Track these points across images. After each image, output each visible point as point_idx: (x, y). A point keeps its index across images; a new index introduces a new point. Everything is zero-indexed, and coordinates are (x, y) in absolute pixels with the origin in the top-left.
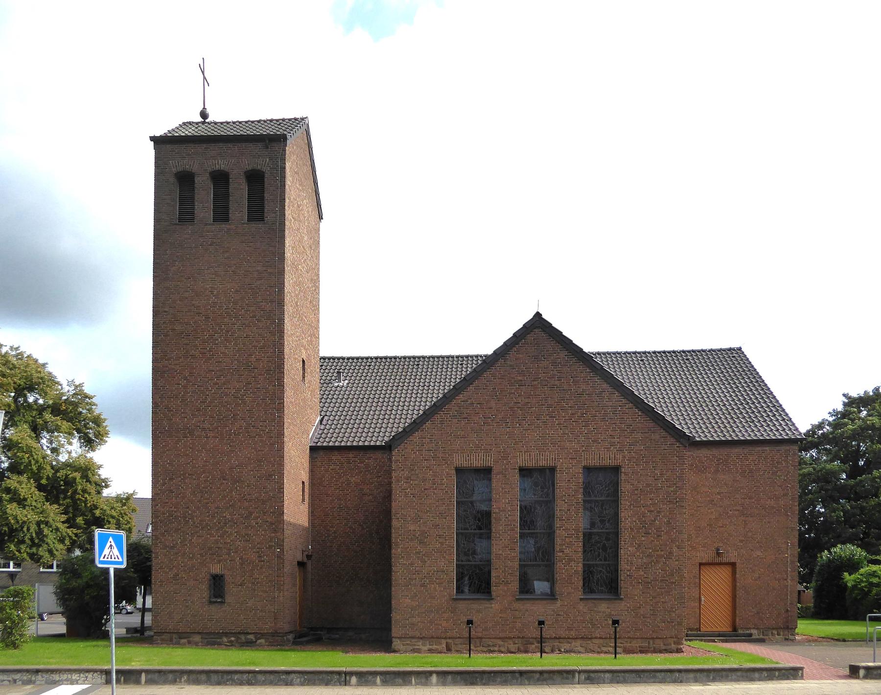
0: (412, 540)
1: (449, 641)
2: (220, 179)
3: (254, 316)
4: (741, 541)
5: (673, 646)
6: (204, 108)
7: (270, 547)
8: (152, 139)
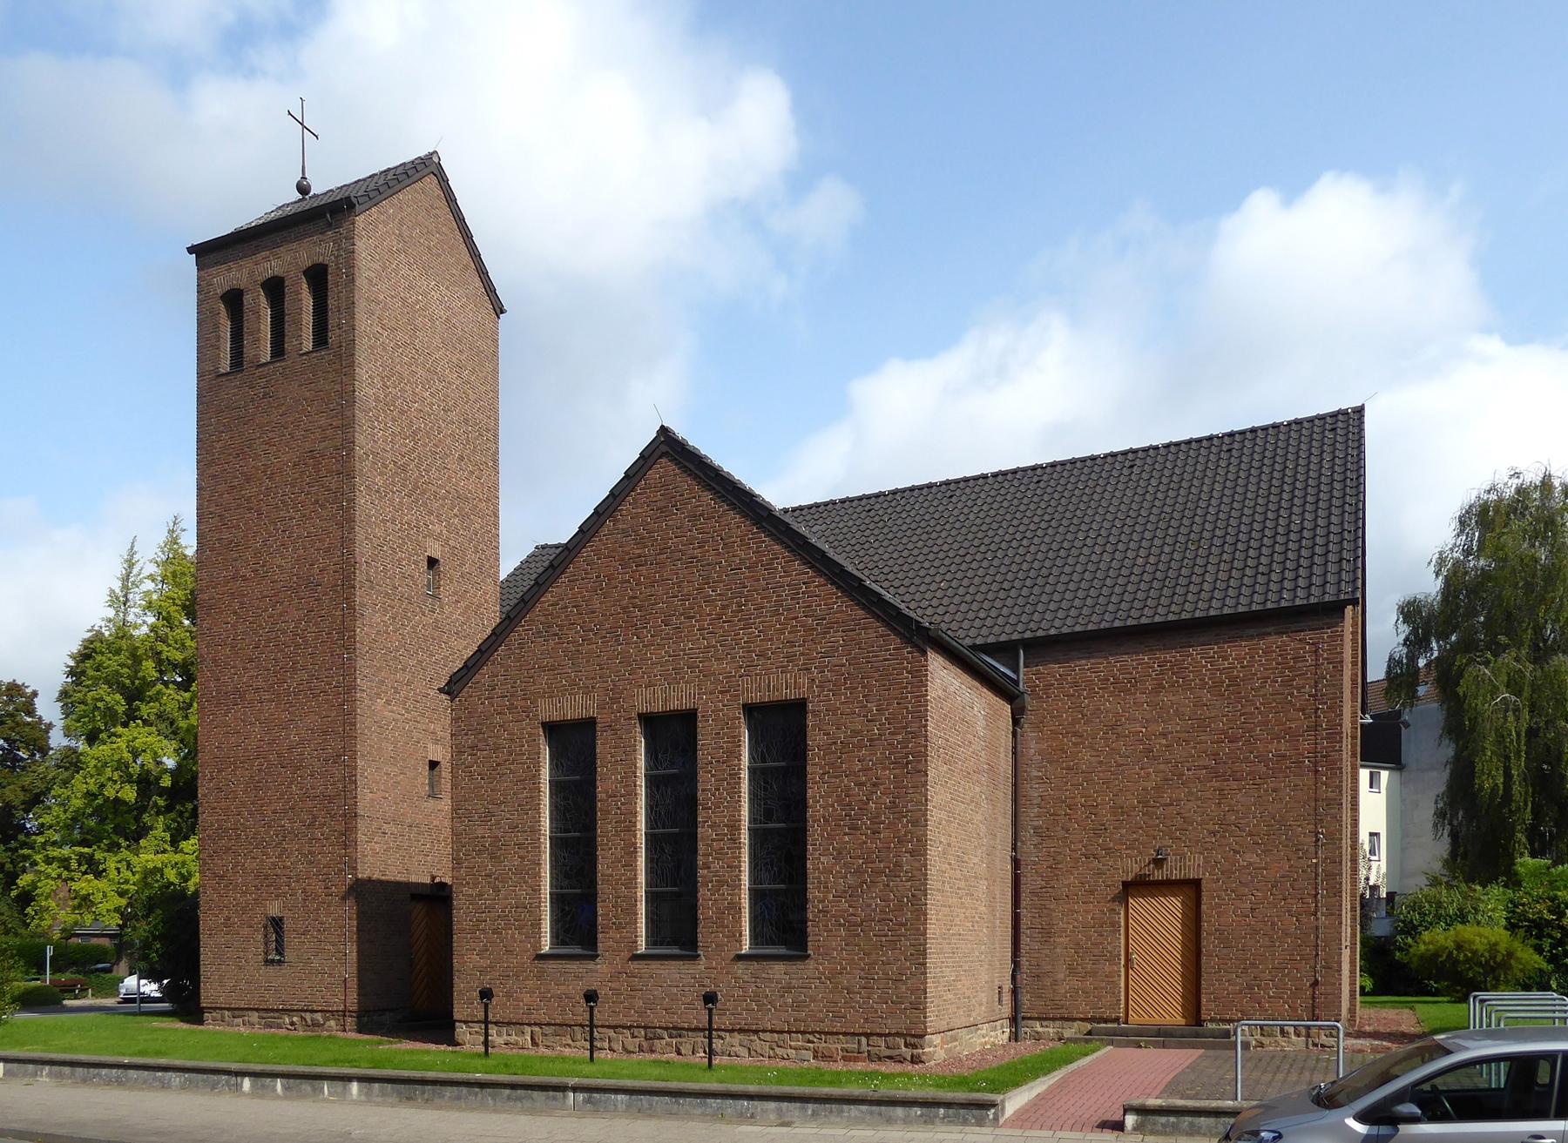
0: (480, 853)
1: (536, 1029)
2: (275, 289)
3: (317, 502)
4: (1214, 833)
5: (907, 1052)
6: (304, 178)
7: (341, 870)
8: (191, 250)
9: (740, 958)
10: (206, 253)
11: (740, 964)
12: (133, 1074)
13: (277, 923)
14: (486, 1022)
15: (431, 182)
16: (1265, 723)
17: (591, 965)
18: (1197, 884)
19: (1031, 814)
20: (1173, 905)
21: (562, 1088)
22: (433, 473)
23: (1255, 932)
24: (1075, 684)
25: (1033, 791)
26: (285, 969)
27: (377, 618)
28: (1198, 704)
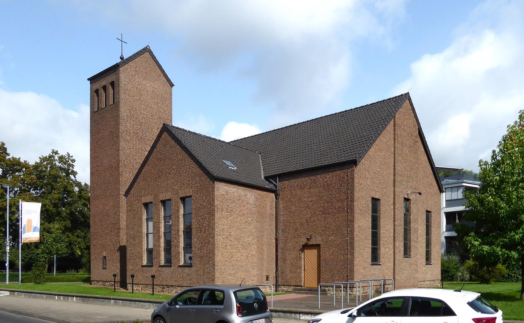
2: (104, 88)
8: (88, 80)
9: (160, 266)
10: (93, 80)
11: (179, 268)
12: (38, 295)
13: (105, 257)
14: (133, 284)
15: (147, 54)
16: (335, 197)
17: (152, 268)
18: (319, 245)
19: (281, 225)
20: (315, 252)
21: (110, 299)
22: (148, 134)
23: (333, 260)
24: (291, 187)
25: (281, 218)
26: (106, 270)
27: (127, 175)
28: (320, 192)
